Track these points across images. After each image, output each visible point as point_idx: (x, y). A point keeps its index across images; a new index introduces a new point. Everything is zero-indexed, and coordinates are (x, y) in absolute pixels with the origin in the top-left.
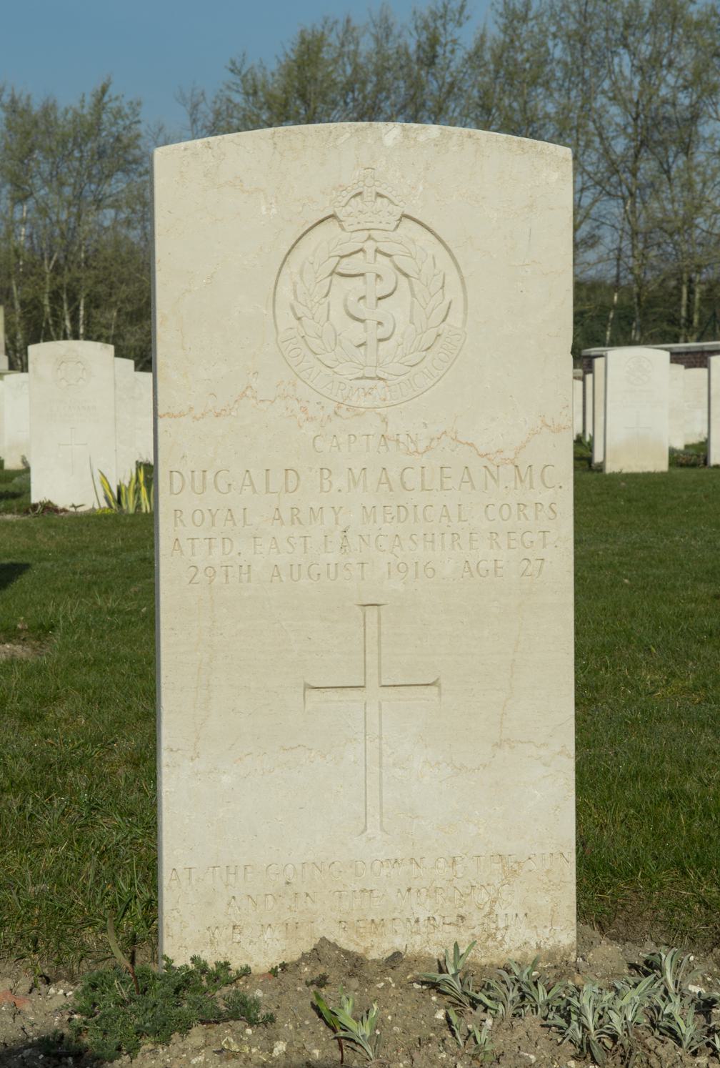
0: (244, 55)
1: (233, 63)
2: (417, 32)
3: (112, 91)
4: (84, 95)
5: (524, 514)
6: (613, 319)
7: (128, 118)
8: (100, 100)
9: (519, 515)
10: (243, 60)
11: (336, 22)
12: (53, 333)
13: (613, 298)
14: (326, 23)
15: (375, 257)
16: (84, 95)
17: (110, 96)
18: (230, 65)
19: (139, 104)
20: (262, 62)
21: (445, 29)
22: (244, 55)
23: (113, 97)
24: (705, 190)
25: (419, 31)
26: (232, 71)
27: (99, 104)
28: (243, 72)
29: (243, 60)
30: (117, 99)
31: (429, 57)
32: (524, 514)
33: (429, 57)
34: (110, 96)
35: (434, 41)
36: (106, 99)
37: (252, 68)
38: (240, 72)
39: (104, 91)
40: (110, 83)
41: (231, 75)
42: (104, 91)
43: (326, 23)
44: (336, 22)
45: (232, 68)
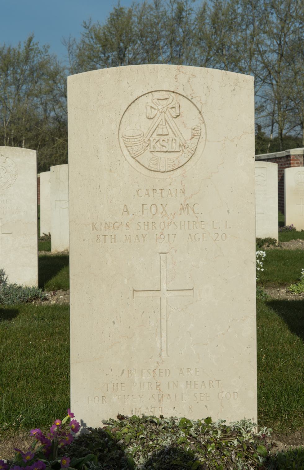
0: (90, 19)
1: (85, 23)
2: (171, 4)
3: (34, 41)
4: (20, 42)
5: (155, 227)
6: (270, 147)
7: (43, 53)
8: (29, 45)
9: (152, 228)
10: (90, 22)
11: (138, 4)
12: (13, 144)
13: (270, 145)
14: (133, 5)
15: (151, 110)
16: (20, 42)
17: (33, 43)
18: (83, 25)
19: (48, 47)
20: (98, 23)
21: (187, 4)
22: (90, 19)
23: (35, 43)
24: (282, 159)
25: (172, 3)
26: (85, 27)
27: (29, 49)
28: (90, 28)
29: (90, 22)
30: (36, 44)
31: (179, 18)
32: (155, 227)
33: (179, 18)
34: (33, 43)
35: (181, 10)
36: (31, 44)
37: (94, 26)
38: (88, 28)
39: (30, 40)
40: (33, 37)
41: (84, 29)
42: (30, 40)
43: (133, 5)
44: (138, 4)
45: (85, 25)
